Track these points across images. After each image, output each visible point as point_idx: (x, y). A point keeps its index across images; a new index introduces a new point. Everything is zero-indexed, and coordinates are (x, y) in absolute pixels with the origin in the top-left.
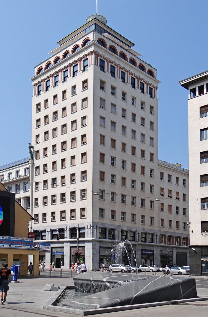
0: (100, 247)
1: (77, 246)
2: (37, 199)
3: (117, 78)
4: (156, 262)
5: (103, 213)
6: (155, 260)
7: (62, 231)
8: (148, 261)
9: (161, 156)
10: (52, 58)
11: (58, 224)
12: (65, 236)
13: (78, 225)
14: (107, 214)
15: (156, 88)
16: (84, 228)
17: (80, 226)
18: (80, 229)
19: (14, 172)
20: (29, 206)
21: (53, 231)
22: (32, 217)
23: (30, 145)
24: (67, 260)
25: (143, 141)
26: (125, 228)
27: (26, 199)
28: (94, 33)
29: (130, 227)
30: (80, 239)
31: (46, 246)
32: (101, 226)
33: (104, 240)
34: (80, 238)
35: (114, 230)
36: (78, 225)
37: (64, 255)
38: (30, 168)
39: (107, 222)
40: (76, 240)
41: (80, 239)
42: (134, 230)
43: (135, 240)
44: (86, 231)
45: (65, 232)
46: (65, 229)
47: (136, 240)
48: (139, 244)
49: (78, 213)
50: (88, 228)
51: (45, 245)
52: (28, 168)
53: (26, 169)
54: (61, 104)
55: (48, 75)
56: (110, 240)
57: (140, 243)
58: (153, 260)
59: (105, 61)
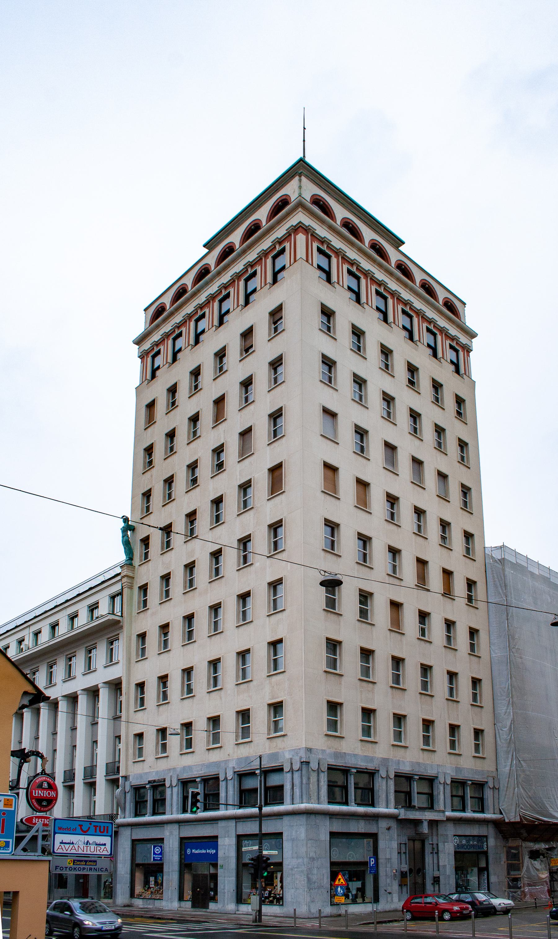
0: (333, 835)
1: (257, 831)
2: (141, 686)
3: (365, 306)
4: (495, 874)
5: (371, 665)
6: (491, 869)
7: (211, 782)
8: (473, 878)
9: (493, 536)
10: (189, 274)
11: (198, 761)
12: (222, 800)
13: (260, 758)
14: (351, 719)
15: (468, 350)
16: (280, 770)
17: (266, 764)
18: (266, 773)
19: (82, 609)
20: (121, 712)
21: (185, 783)
22: (32, 683)
23: (124, 522)
24: (227, 882)
25: (420, 531)
26: (406, 769)
27: (114, 687)
28: (300, 181)
29: (418, 764)
30: (267, 809)
31: (91, 839)
32: (332, 762)
33: (344, 808)
34: (266, 804)
35: (372, 774)
36: (260, 758)
37: (220, 862)
38: (126, 591)
39: (352, 748)
40: (255, 810)
41: (267, 809)
42: (431, 772)
43: (436, 807)
44: (285, 780)
45: (222, 785)
46: (222, 777)
47: (438, 805)
48: (449, 819)
49: (260, 719)
50: (292, 771)
51: (85, 833)
52: (120, 594)
53: (113, 598)
54: (234, 581)
55: (178, 318)
56: (361, 809)
57: (449, 814)
58: (487, 869)
59: (333, 256)
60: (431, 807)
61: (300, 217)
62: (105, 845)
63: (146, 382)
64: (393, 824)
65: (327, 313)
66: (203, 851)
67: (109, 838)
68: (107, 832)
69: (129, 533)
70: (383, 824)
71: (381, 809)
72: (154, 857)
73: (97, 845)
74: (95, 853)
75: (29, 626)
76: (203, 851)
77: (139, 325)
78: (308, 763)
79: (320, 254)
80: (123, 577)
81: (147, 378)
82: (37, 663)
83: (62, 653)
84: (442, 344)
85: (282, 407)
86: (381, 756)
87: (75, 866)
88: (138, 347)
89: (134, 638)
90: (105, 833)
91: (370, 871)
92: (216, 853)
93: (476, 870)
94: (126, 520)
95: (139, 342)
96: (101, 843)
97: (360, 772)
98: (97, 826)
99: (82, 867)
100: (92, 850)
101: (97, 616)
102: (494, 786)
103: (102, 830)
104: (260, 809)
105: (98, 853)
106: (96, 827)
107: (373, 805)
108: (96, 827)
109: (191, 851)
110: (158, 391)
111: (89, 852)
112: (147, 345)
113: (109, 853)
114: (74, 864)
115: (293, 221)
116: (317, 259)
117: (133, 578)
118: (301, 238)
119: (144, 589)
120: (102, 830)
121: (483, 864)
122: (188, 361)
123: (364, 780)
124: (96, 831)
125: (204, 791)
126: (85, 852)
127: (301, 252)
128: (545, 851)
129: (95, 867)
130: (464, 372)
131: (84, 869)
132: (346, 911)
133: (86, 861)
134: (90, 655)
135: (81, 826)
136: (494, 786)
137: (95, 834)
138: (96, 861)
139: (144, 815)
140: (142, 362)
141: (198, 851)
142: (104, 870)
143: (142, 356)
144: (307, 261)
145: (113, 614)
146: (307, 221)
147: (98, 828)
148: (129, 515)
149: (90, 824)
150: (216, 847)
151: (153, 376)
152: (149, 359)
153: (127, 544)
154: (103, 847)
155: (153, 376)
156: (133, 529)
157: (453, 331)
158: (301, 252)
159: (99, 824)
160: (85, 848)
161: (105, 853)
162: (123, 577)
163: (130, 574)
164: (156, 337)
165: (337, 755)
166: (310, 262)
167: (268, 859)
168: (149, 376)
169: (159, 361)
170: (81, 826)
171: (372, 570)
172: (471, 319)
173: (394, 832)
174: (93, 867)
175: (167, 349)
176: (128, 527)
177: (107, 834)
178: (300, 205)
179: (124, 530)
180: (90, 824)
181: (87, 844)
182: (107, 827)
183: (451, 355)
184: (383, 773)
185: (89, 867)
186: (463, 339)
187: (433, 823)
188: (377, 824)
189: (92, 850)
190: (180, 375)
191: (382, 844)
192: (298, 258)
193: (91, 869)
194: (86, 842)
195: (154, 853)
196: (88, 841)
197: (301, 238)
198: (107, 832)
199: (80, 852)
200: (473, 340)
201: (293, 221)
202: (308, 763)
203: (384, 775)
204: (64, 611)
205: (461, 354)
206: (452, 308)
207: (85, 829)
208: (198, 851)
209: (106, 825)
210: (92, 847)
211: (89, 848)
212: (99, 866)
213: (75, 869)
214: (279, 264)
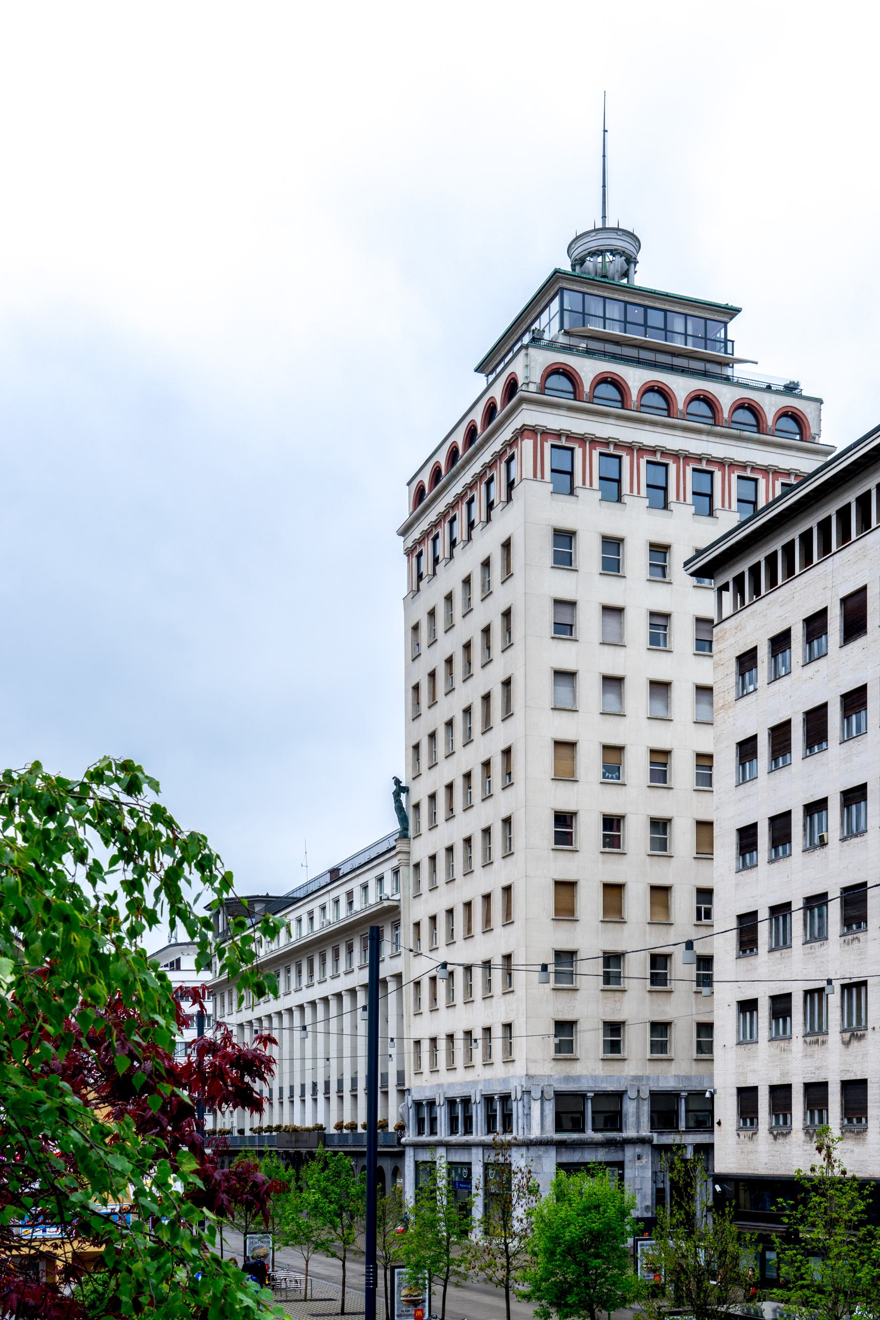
29: (688, 1078)
39: (590, 1070)
56: (599, 1136)
64: (646, 1153)
70: (630, 1153)
71: (630, 1133)
75: (328, 891)
77: (403, 510)
80: (398, 853)
82: (336, 941)
83: (357, 932)
86: (632, 1073)
88: (402, 539)
89: (412, 926)
94: (397, 782)
95: (404, 532)
97: (601, 1096)
107: (620, 1130)
117: (409, 853)
119: (417, 866)
125: (459, 1108)
128: (64, 1189)
153: (400, 809)
156: (406, 790)
162: (398, 853)
163: (405, 849)
165: (568, 1079)
168: (415, 588)
173: (647, 1160)
176: (400, 789)
179: (397, 795)
184: (632, 1094)
188: (623, 1151)
191: (628, 1173)
197: (527, 445)
201: (516, 423)
204: (356, 879)
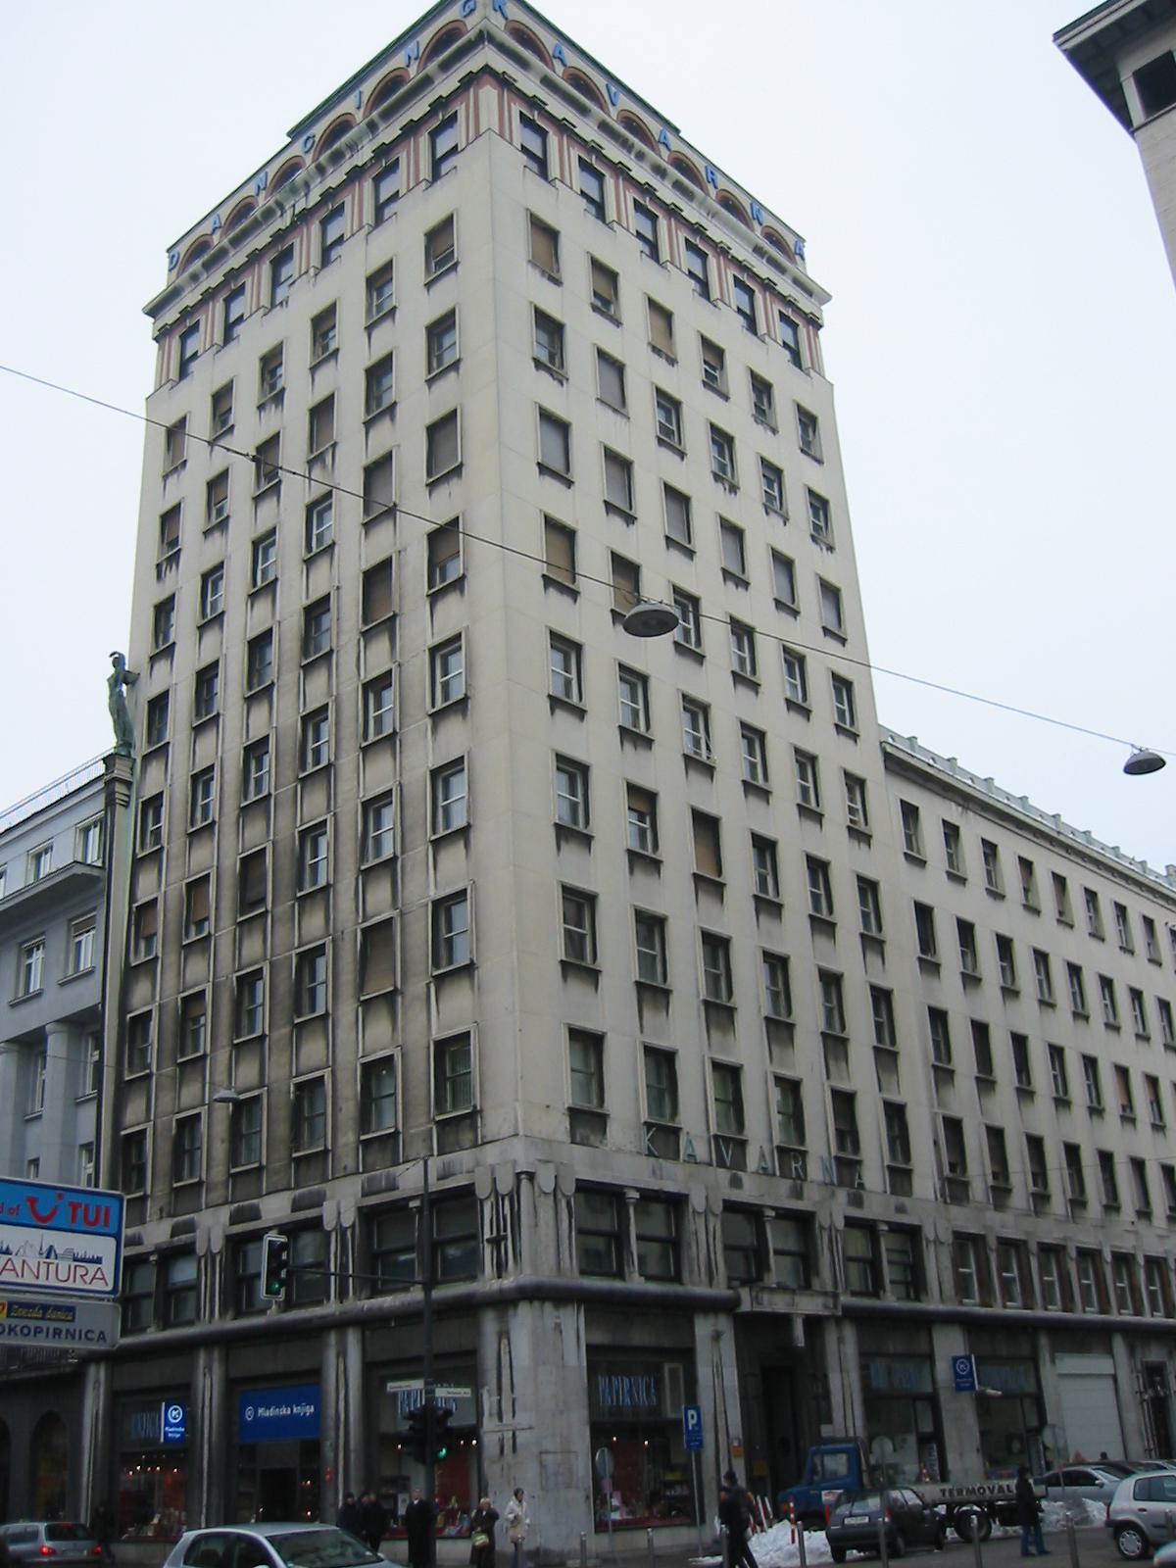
15: (815, 323)
31: (62, 1241)
51: (43, 1222)
55: (236, 260)
60: (806, 1286)
61: (487, 56)
62: (98, 1261)
63: (169, 385)
65: (545, 234)
66: (285, 1411)
67: (112, 1242)
68: (106, 1224)
69: (124, 687)
72: (166, 1433)
73: (75, 1260)
74: (70, 1284)
76: (285, 1411)
78: (531, 1176)
79: (525, 126)
81: (171, 377)
84: (766, 310)
85: (455, 411)
87: (14, 1322)
88: (152, 320)
90: (99, 1228)
91: (688, 1442)
92: (319, 1415)
93: (912, 1440)
95: (154, 311)
96: (89, 1256)
98: (79, 1205)
99: (32, 1324)
100: (63, 1276)
101: (48, 871)
102: (937, 1236)
103: (92, 1216)
104: (428, 1287)
105: (79, 1285)
106: (75, 1206)
108: (75, 1206)
109: (256, 1412)
110: (194, 401)
111: (53, 1282)
112: (171, 315)
113: (109, 1288)
114: (8, 1316)
115: (473, 63)
116: (521, 135)
118: (489, 94)
120: (92, 1216)
121: (927, 1427)
122: (254, 340)
123: (657, 1225)
124: (74, 1219)
126: (42, 1281)
127: (489, 117)
129: (71, 1326)
130: (810, 365)
131: (38, 1330)
132: (650, 1541)
133: (45, 1308)
134: (29, 962)
135: (32, 1201)
136: (937, 1236)
137: (74, 1227)
138: (71, 1309)
139: (143, 1330)
140: (161, 348)
141: (271, 1413)
142: (95, 1336)
143: (161, 336)
144: (501, 135)
145: (83, 864)
146: (501, 64)
147: (80, 1213)
148: (125, 651)
149: (60, 1197)
150: (316, 1398)
151: (183, 372)
152: (176, 341)
153: (118, 710)
154: (92, 1268)
155: (183, 372)
157: (785, 287)
158: (489, 117)
159: (84, 1200)
160: (43, 1268)
161: (98, 1285)
164: (190, 298)
166: (508, 137)
167: (448, 1413)
168: (174, 373)
169: (194, 344)
170: (32, 1201)
171: (642, 753)
172: (816, 267)
174: (64, 1326)
175: (212, 320)
176: (122, 677)
177: (106, 1231)
178: (484, 37)
179: (115, 682)
180: (60, 1197)
181: (48, 1257)
182: (107, 1210)
183: (783, 332)
185: (53, 1325)
186: (806, 304)
187: (813, 1324)
189: (63, 1276)
190: (240, 364)
192: (483, 129)
193: (57, 1333)
194: (45, 1249)
195: (167, 1423)
196: (51, 1247)
197: (489, 94)
198: (106, 1224)
199: (28, 1279)
200: (823, 307)
201: (473, 63)
202: (531, 1176)
203: (701, 1208)
205: (802, 330)
206: (782, 245)
207: (44, 1212)
208: (271, 1413)
209: (104, 1202)
210: (63, 1266)
211: (52, 1268)
212: (82, 1323)
213: (12, 1330)
214: (444, 144)
